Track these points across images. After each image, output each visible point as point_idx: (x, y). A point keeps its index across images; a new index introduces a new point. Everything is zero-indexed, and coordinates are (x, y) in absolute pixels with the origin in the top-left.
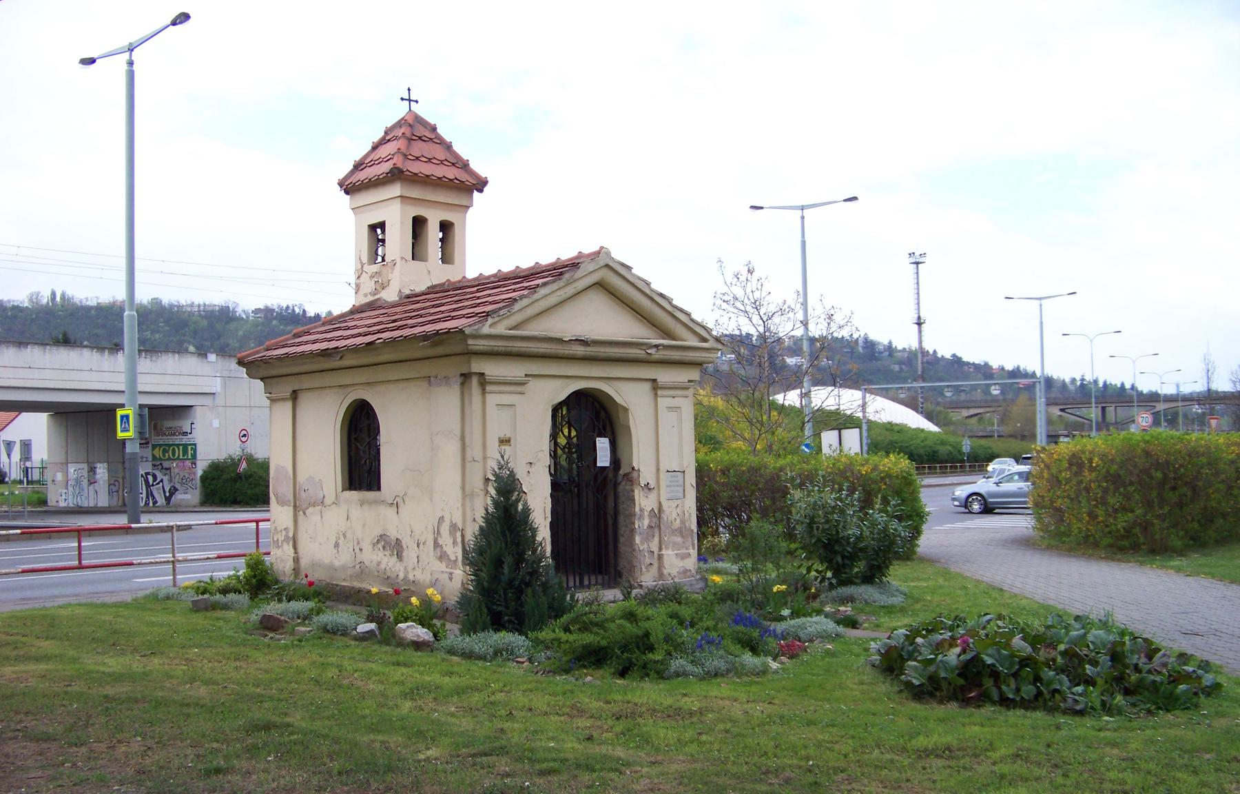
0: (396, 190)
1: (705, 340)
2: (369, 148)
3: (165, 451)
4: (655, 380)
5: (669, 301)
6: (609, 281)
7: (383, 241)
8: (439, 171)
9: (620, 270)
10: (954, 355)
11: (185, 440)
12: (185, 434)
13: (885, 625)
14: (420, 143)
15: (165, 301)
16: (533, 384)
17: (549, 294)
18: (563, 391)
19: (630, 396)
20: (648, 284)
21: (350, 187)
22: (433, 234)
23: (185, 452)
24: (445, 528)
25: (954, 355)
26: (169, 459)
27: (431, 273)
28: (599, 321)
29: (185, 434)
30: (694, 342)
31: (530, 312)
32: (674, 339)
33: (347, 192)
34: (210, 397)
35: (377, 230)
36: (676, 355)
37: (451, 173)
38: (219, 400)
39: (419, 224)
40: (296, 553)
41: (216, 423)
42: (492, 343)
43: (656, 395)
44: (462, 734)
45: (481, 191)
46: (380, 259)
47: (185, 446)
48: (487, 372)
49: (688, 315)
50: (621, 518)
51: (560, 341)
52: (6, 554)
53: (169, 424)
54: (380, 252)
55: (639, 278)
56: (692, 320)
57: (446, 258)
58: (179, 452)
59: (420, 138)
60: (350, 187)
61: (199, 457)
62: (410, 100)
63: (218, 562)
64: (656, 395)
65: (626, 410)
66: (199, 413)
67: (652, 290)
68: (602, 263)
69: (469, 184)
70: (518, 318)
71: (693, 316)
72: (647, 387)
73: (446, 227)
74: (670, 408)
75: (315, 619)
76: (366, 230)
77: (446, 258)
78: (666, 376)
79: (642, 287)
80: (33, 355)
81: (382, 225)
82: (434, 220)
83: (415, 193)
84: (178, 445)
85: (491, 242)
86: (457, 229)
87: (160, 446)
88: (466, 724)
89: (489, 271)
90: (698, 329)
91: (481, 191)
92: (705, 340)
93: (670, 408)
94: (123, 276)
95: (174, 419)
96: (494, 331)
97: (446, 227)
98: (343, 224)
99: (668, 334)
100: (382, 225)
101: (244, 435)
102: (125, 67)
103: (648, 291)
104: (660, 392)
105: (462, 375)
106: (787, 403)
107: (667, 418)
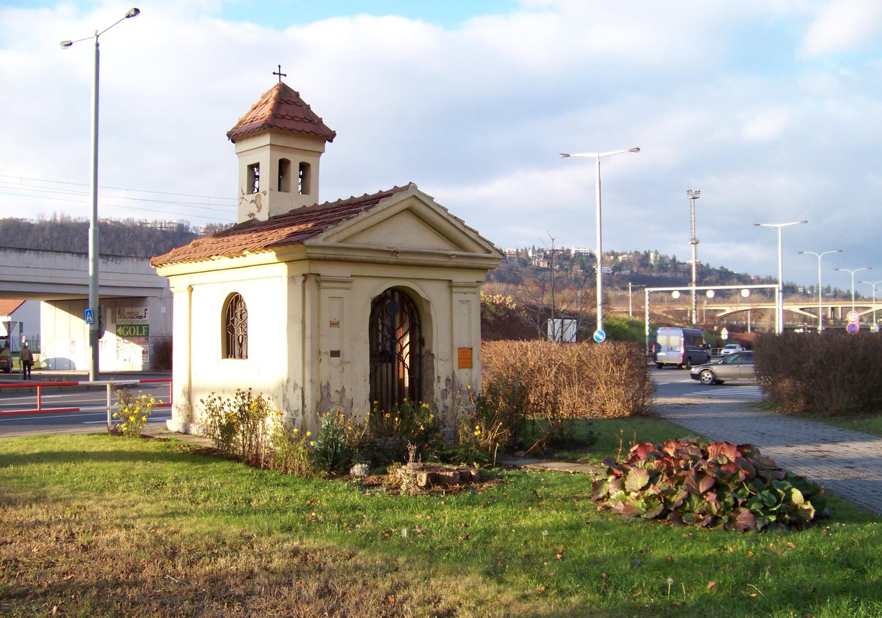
0: (266, 140)
1: (489, 252)
2: (250, 109)
4: (450, 281)
5: (462, 222)
6: (417, 208)
7: (258, 177)
8: (299, 126)
10: (722, 267)
11: (140, 322)
12: (141, 317)
14: (287, 106)
15: (7, 218)
16: (357, 283)
17: (364, 218)
18: (379, 288)
19: (431, 291)
20: (446, 210)
21: (235, 137)
22: (294, 171)
23: (141, 330)
24: (291, 385)
27: (294, 200)
28: (410, 236)
29: (141, 317)
30: (480, 253)
31: (355, 229)
33: (233, 142)
35: (253, 168)
37: (308, 128)
39: (283, 165)
40: (190, 404)
42: (339, 252)
43: (451, 292)
45: (331, 141)
46: (256, 190)
47: (141, 326)
48: (322, 274)
49: (477, 233)
50: (424, 384)
52: (3, 402)
53: (128, 310)
54: (257, 186)
56: (479, 237)
57: (305, 190)
60: (235, 137)
61: (150, 335)
62: (280, 74)
64: (451, 292)
65: (428, 302)
66: (150, 301)
67: (449, 215)
68: (410, 195)
69: (322, 135)
70: (341, 236)
71: (480, 234)
72: (443, 286)
73: (304, 167)
74: (462, 302)
76: (246, 169)
77: (305, 190)
78: (459, 278)
79: (441, 211)
80: (29, 257)
81: (257, 165)
82: (295, 162)
83: (281, 142)
84: (135, 326)
85: (338, 177)
86: (312, 169)
87: (123, 326)
89: (332, 200)
91: (331, 141)
92: (489, 252)
93: (462, 302)
97: (304, 167)
98: (231, 162)
99: (460, 246)
100: (257, 165)
102: (94, 47)
104: (454, 290)
105: (304, 275)
107: (460, 310)
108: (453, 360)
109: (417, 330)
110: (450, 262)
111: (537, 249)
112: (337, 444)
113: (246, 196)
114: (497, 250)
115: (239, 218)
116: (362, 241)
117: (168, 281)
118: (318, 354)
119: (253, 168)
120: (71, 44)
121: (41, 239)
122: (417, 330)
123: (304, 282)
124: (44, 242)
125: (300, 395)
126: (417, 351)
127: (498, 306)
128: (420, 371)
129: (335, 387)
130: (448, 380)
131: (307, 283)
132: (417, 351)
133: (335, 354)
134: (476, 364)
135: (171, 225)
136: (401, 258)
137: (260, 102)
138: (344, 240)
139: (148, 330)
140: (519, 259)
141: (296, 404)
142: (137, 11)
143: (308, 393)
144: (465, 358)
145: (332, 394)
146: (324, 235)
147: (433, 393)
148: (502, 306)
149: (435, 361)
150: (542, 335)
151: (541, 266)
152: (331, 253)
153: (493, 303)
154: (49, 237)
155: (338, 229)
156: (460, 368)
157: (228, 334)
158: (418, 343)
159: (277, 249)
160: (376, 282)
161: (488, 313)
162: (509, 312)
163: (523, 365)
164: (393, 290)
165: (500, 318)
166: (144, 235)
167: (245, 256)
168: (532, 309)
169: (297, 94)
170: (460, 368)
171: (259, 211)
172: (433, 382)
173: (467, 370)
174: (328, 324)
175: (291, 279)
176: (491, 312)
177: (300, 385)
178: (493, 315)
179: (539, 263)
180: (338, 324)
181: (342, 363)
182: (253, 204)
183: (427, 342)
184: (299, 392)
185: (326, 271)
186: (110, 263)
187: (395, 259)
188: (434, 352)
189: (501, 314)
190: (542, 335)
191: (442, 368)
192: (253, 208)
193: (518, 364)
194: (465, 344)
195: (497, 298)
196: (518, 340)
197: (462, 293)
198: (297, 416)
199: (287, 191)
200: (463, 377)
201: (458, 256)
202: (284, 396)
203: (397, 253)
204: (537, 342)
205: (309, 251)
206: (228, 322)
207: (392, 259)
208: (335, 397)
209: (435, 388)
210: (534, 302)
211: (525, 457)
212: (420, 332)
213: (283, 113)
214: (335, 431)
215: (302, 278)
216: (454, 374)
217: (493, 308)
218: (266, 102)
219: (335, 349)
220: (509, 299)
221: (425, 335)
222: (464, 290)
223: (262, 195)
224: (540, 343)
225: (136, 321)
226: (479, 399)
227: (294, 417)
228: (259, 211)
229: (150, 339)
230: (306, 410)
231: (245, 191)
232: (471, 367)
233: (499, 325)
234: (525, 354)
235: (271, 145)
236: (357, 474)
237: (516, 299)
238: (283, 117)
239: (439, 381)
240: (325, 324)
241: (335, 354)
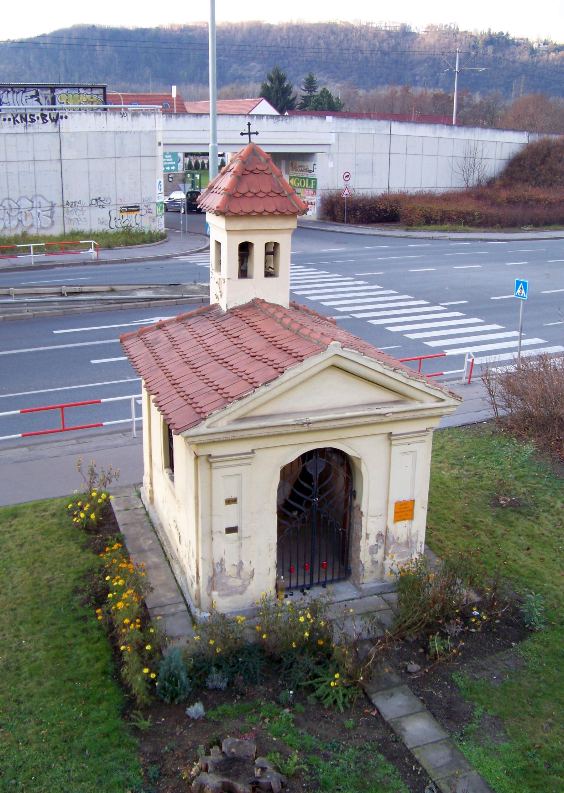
1: (443, 400)
3: (297, 182)
11: (309, 175)
12: (310, 171)
14: (252, 177)
18: (292, 454)
23: (310, 183)
26: (300, 187)
29: (310, 171)
34: (328, 146)
38: (333, 149)
39: (245, 249)
41: (331, 165)
43: (391, 444)
44: (511, 373)
47: (310, 180)
53: (299, 163)
58: (306, 183)
61: (318, 188)
66: (319, 157)
70: (251, 406)
83: (240, 225)
84: (305, 179)
87: (295, 177)
92: (443, 400)
95: (303, 160)
101: (347, 176)
106: (263, 781)
108: (387, 514)
121: (279, 40)
124: (281, 42)
129: (230, 561)
133: (230, 530)
135: (395, 25)
139: (316, 183)
145: (228, 567)
146: (208, 422)
147: (358, 550)
154: (286, 37)
160: (287, 449)
166: (370, 35)
172: (360, 539)
173: (406, 522)
174: (224, 502)
181: (240, 538)
183: (358, 495)
186: (280, 122)
194: (405, 497)
197: (404, 444)
207: (306, 428)
216: (387, 529)
221: (357, 488)
225: (306, 175)
229: (318, 193)
240: (219, 501)
241: (230, 530)
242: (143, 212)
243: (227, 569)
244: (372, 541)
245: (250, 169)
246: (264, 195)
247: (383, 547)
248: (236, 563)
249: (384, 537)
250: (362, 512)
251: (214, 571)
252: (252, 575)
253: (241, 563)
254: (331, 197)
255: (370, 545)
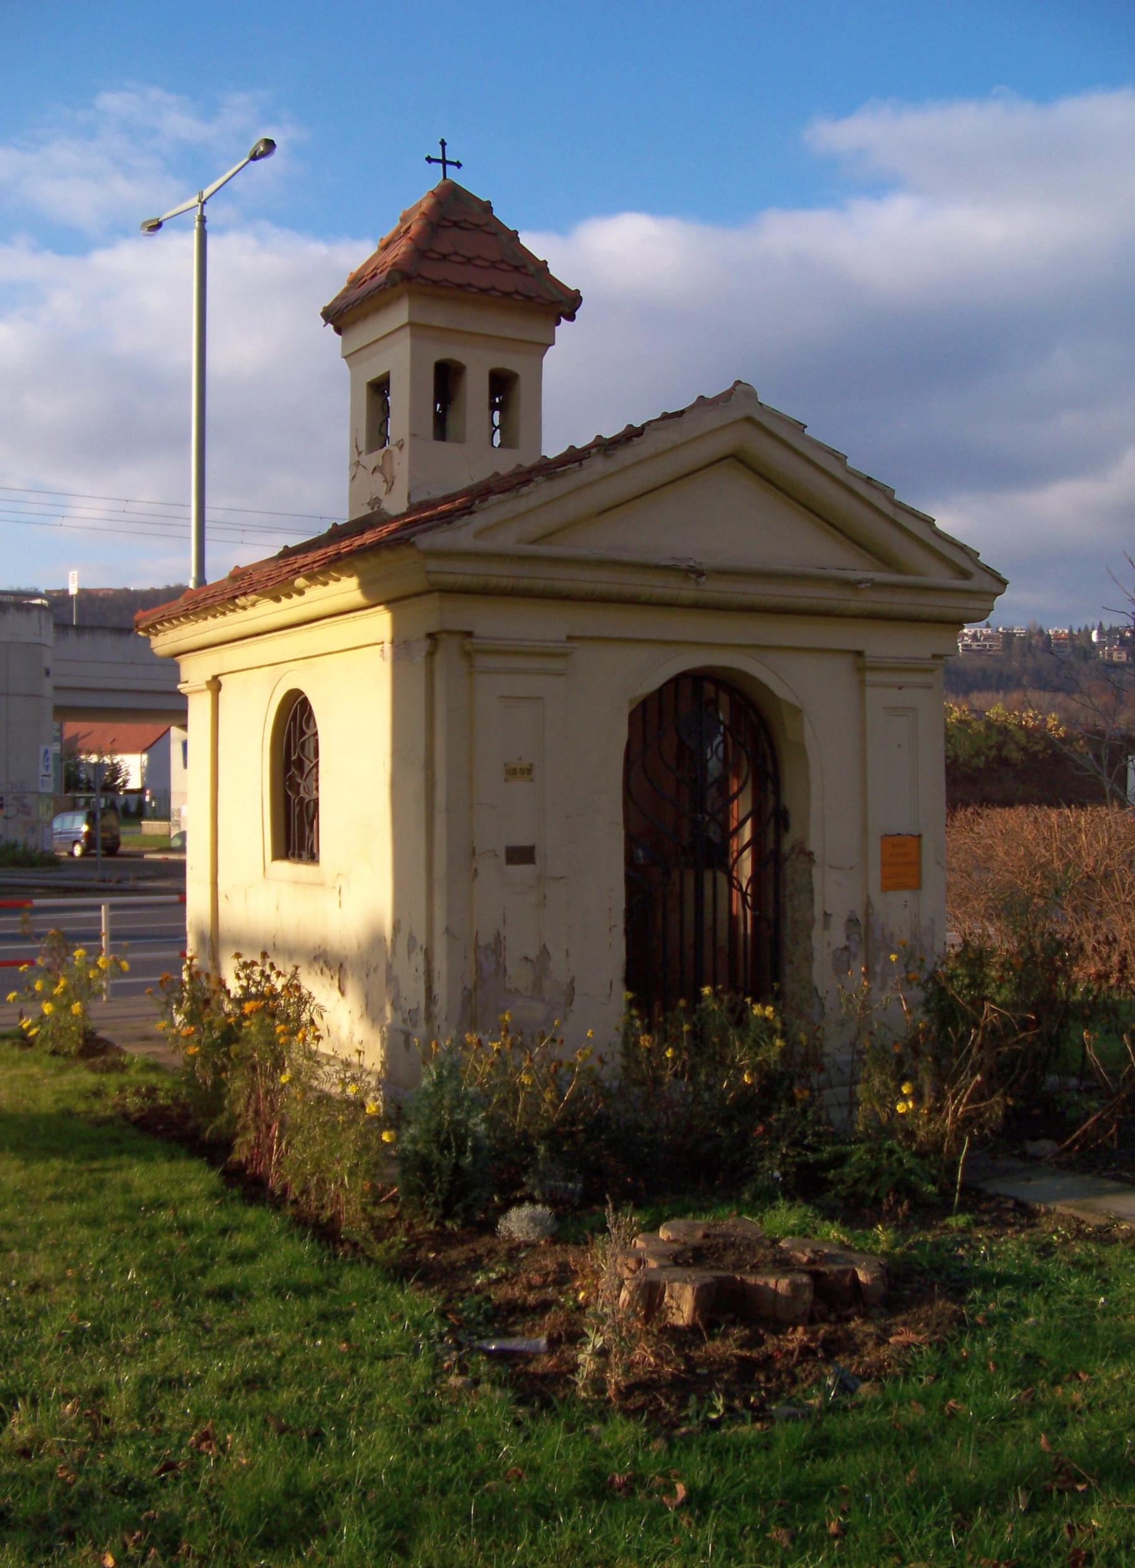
0: (400, 314)
1: (965, 575)
4: (859, 654)
8: (484, 280)
9: (785, 433)
13: (545, 1359)
15: (172, 585)
18: (654, 671)
19: (803, 680)
20: (840, 458)
22: (475, 388)
25: (578, 291)
30: (941, 577)
32: (900, 571)
35: (380, 388)
36: (902, 603)
37: (507, 282)
39: (447, 379)
43: (862, 683)
45: (571, 317)
48: (477, 631)
51: (696, 573)
55: (820, 447)
59: (456, 224)
62: (444, 162)
63: (87, 884)
64: (862, 683)
65: (797, 712)
68: (737, 414)
73: (502, 385)
75: (943, 984)
76: (363, 392)
78: (881, 644)
79: (828, 463)
83: (440, 316)
86: (523, 387)
88: (475, 1193)
90: (947, 550)
91: (571, 317)
92: (965, 575)
94: (208, 503)
96: (483, 545)
99: (887, 561)
103: (838, 472)
104: (870, 677)
109: (770, 787)
110: (856, 602)
111: (1106, 628)
112: (461, 1140)
113: (366, 459)
114: (987, 570)
115: (351, 512)
116: (602, 540)
117: (177, 666)
118: (466, 860)
119: (380, 388)
120: (159, 225)
122: (770, 787)
123: (431, 654)
125: (422, 968)
126: (771, 845)
127: (1029, 733)
128: (777, 901)
130: (852, 922)
131: (438, 657)
132: (771, 845)
133: (521, 855)
134: (933, 877)
136: (713, 589)
137: (397, 232)
138: (545, 537)
140: (1074, 647)
141: (415, 994)
142: (270, 144)
143: (440, 965)
144: (902, 862)
147: (809, 958)
148: (1037, 733)
149: (815, 871)
150: (1113, 794)
151: (1115, 659)
152: (501, 575)
153: (1021, 727)
155: (522, 505)
156: (885, 889)
157: (287, 798)
158: (773, 818)
159: (361, 565)
161: (1011, 745)
162: (1050, 743)
163: (1067, 865)
164: (695, 679)
165: (1035, 754)
167: (301, 592)
168: (1096, 737)
169: (487, 207)
170: (885, 889)
171: (389, 490)
173: (906, 895)
175: (401, 647)
176: (1017, 743)
177: (421, 939)
178: (1024, 749)
179: (1110, 655)
180: (529, 771)
182: (378, 475)
183: (794, 820)
184: (419, 959)
185: (492, 622)
187: (691, 589)
188: (813, 846)
189: (1036, 748)
190: (1113, 794)
191: (836, 887)
192: (377, 485)
193: (1057, 864)
195: (1029, 718)
196: (1059, 806)
198: (415, 1025)
199: (460, 440)
200: (895, 912)
201: (876, 585)
202: (389, 967)
203: (700, 574)
204: (1103, 811)
205: (433, 565)
206: (287, 769)
207: (688, 591)
208: (519, 976)
209: (815, 943)
210: (1101, 724)
211: (1067, 1165)
212: (777, 793)
213: (445, 250)
214: (459, 1099)
215: (424, 645)
216: (869, 905)
217: (1020, 736)
218: (407, 231)
219: (521, 840)
220: (1052, 720)
222: (897, 678)
223: (396, 450)
224: (1109, 814)
226: (933, 977)
227: (409, 1028)
228: (389, 490)
230: (436, 1010)
231: (363, 447)
232: (916, 885)
233: (985, 775)
234: (1074, 839)
235: (411, 324)
236: (519, 1236)
237: (1069, 720)
238: (445, 257)
239: (826, 927)
241: (521, 855)
242: (11, 811)
243: (510, 971)
244: (838, 936)
245: (454, 218)
246: (488, 264)
247: (861, 956)
248: (532, 953)
249: (862, 928)
250: (810, 854)
251: (479, 969)
252: (570, 993)
253: (545, 952)
254: (325, 951)
255: (833, 948)
